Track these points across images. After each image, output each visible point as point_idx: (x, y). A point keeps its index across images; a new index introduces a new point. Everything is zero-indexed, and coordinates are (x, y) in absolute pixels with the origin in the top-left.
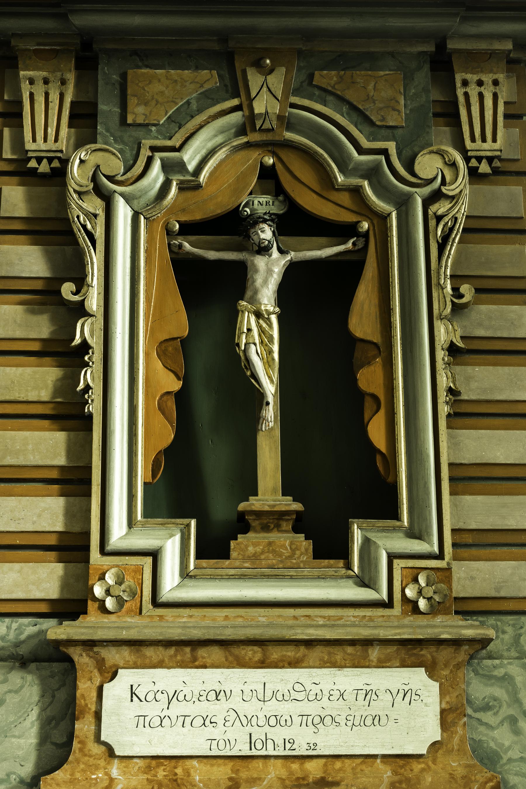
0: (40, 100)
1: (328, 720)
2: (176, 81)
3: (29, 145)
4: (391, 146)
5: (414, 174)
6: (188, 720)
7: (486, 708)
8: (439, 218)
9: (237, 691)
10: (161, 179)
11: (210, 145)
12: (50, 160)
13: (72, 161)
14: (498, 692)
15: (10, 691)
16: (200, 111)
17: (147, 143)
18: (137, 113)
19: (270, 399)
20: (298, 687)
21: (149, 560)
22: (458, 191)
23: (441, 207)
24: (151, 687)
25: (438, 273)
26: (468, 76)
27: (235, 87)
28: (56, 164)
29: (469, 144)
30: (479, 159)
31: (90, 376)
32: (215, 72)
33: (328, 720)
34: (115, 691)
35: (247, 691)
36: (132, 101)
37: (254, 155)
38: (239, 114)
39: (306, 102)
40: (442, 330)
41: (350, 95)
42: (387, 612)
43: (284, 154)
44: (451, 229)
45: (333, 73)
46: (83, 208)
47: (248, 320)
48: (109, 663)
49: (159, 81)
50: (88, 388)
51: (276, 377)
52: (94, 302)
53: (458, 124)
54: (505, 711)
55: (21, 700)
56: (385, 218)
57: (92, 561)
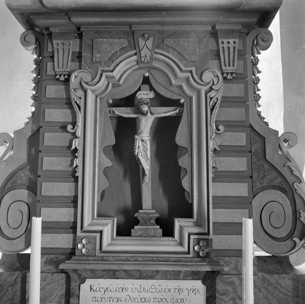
0: (61, 51)
1: (164, 300)
2: (112, 44)
3: (57, 70)
4: (193, 69)
5: (202, 81)
6: (112, 299)
7: (224, 294)
8: (211, 99)
9: (130, 288)
10: (106, 83)
11: (125, 69)
12: (232, 74)
13: (245, 238)
14: (229, 288)
15: (47, 284)
16: (120, 56)
17: (100, 69)
18: (97, 56)
19: (147, 172)
20: (153, 287)
21: (99, 234)
22: (218, 88)
23: (212, 94)
24: (98, 286)
25: (210, 121)
26: (230, 40)
27: (134, 46)
28: (66, 77)
29: (223, 68)
30: (227, 74)
31: (78, 162)
32: (126, 40)
33: (164, 300)
34: (85, 287)
35: (134, 288)
36: (95, 52)
37: (142, 72)
38: (136, 56)
39: (161, 52)
40: (212, 143)
41: (177, 48)
42: (188, 256)
43: (154, 72)
44: (216, 103)
45: (172, 39)
46: (76, 95)
47: (138, 143)
48: (83, 276)
49: (105, 43)
50: (77, 166)
51: (149, 163)
52: (79, 133)
53: (219, 59)
54: (231, 296)
55: (51, 288)
56: (191, 98)
57: (77, 235)
